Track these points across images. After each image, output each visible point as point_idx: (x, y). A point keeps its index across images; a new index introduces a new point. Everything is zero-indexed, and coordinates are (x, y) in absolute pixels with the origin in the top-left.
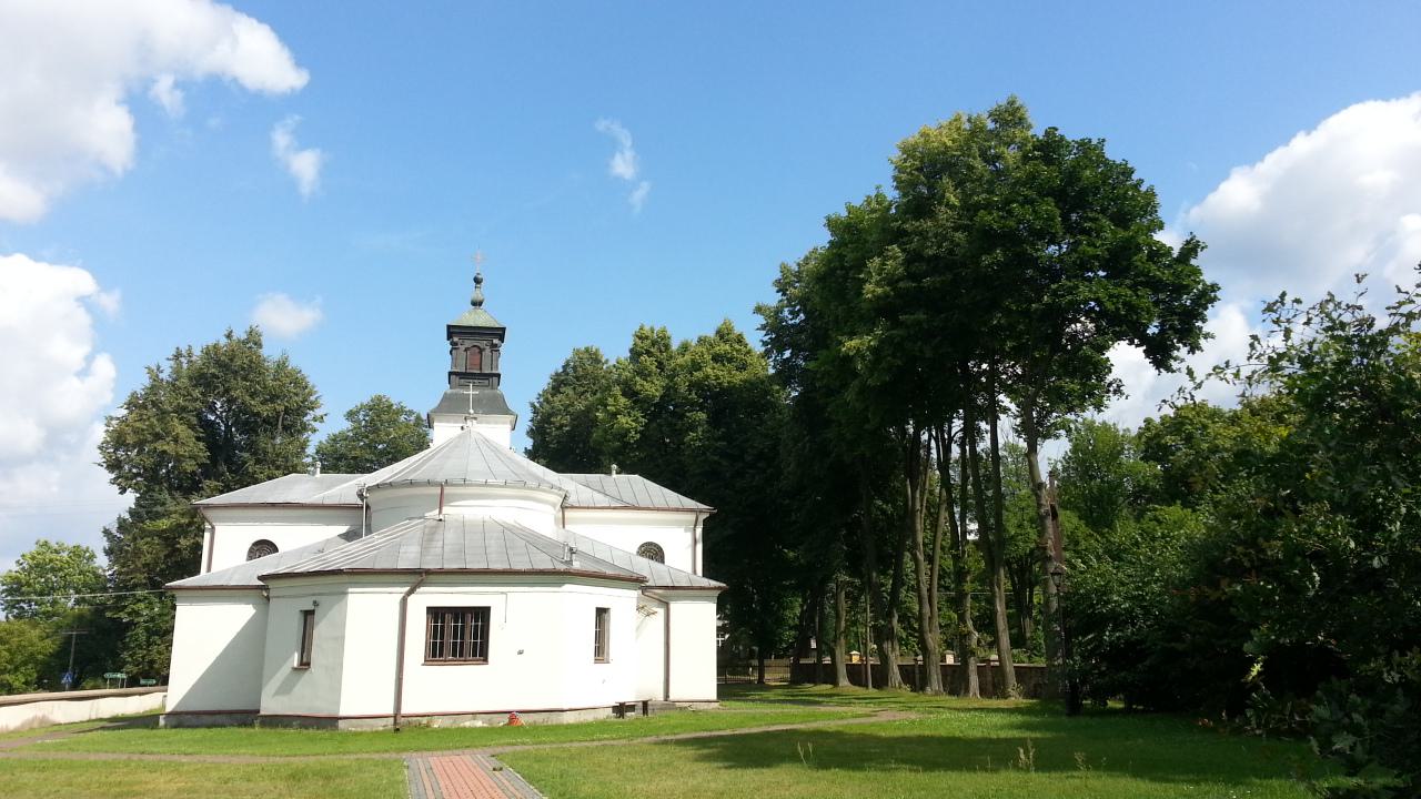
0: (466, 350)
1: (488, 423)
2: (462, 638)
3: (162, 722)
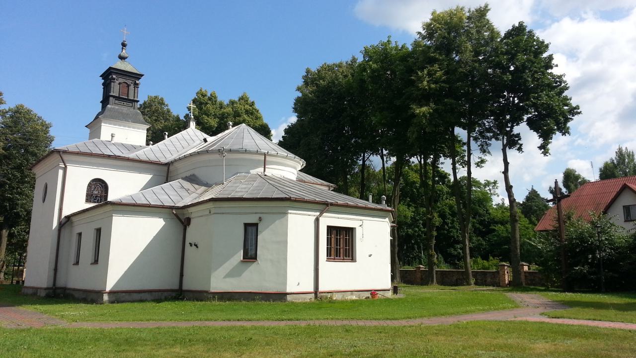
0: (120, 84)
1: (134, 128)
2: (340, 246)
3: (106, 297)
